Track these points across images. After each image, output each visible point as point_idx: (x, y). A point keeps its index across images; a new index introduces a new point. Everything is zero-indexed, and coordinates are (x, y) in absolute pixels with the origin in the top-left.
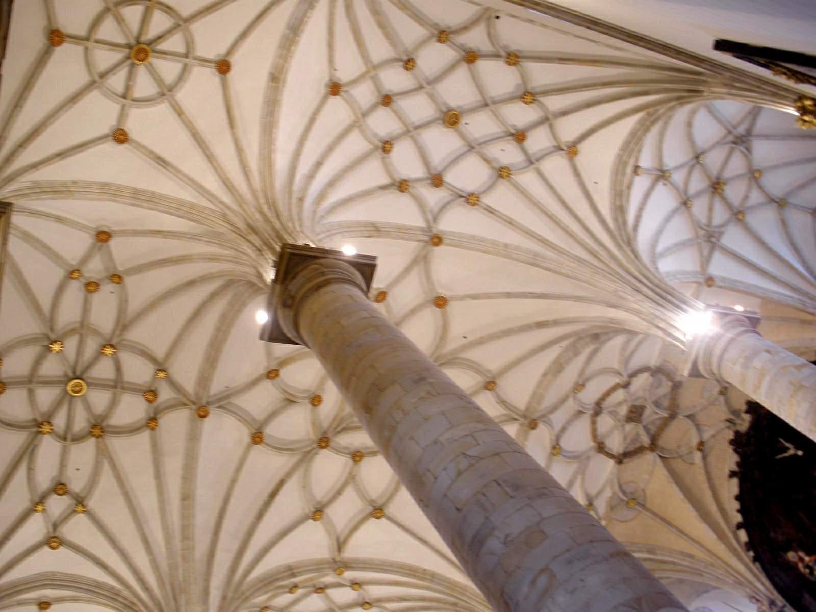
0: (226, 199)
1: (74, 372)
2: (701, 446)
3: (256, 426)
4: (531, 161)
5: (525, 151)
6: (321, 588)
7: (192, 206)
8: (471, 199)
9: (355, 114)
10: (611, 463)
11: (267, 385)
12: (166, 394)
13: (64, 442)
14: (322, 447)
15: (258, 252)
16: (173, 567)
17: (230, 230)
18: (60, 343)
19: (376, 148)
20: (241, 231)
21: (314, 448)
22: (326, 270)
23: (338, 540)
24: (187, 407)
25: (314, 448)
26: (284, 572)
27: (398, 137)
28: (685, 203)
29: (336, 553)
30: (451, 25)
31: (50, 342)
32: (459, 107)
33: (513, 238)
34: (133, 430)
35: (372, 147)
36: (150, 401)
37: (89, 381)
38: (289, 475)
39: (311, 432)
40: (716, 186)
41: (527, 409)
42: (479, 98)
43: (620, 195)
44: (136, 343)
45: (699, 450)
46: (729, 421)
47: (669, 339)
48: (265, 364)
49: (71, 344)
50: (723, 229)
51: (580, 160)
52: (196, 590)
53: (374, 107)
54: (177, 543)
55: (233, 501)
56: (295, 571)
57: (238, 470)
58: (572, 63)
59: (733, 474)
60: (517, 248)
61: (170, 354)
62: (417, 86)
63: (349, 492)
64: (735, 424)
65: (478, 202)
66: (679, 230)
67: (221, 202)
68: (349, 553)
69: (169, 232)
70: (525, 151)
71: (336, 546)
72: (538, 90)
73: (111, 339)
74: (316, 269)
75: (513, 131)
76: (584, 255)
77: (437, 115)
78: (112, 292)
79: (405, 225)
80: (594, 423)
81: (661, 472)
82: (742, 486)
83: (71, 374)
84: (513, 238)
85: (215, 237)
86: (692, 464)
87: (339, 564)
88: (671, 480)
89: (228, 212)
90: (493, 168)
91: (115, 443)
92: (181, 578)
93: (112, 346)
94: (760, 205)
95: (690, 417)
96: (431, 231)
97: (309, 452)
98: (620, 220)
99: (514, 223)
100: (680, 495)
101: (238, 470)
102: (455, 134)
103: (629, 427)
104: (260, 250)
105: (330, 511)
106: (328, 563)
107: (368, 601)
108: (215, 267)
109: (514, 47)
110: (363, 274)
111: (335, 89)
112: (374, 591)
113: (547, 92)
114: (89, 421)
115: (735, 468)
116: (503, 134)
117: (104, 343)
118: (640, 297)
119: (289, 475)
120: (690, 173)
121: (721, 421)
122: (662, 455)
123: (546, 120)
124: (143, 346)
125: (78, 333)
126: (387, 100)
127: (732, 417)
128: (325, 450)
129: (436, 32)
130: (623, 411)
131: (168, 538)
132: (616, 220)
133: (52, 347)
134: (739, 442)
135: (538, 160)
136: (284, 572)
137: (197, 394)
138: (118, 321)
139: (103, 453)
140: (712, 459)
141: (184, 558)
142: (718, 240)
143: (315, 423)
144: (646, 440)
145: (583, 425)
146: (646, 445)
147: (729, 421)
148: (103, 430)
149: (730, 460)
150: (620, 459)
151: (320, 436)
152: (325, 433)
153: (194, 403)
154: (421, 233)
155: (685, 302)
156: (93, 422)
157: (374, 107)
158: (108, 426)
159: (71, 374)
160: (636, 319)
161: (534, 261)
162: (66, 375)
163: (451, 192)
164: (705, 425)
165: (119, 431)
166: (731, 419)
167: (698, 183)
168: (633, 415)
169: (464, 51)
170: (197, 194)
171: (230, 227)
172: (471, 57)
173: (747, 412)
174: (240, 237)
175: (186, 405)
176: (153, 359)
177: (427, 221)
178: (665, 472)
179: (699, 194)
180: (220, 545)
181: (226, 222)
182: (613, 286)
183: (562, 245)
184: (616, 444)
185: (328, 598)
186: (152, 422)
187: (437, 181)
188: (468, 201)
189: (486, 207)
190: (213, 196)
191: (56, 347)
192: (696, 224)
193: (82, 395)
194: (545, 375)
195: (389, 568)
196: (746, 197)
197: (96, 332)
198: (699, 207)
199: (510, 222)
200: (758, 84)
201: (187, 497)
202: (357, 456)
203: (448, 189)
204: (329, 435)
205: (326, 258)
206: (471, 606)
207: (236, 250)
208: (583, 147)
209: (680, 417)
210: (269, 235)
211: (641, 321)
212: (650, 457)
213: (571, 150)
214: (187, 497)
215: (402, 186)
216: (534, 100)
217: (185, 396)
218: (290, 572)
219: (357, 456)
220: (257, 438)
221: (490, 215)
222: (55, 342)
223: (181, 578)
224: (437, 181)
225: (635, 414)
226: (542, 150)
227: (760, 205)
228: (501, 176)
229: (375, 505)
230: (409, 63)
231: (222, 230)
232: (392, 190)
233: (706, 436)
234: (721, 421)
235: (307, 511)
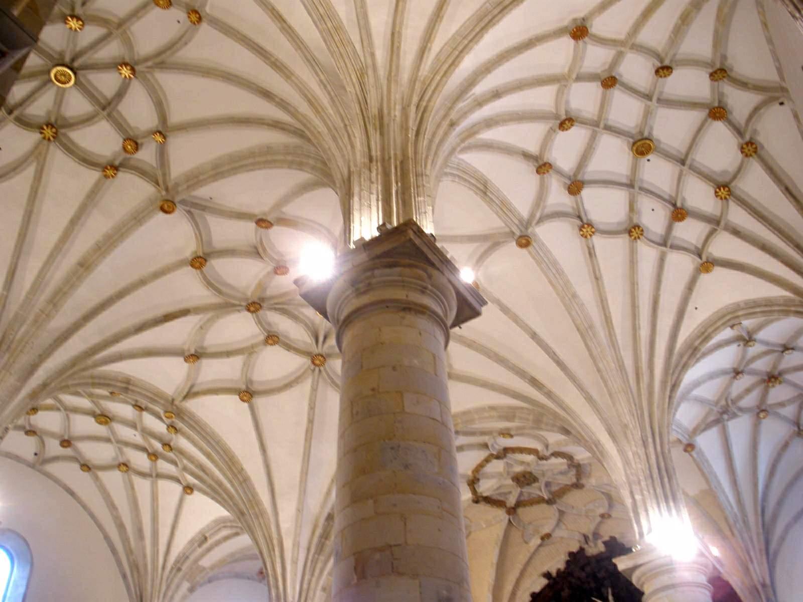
0: (381, 55)
1: (73, 60)
2: (546, 537)
3: (207, 250)
4: (665, 242)
5: (669, 228)
6: (140, 407)
7: (339, 28)
8: (586, 227)
9: (570, 70)
11: (252, 225)
12: (147, 155)
13: (6, 115)
14: (249, 310)
15: (367, 161)
16: (18, 319)
17: (356, 94)
18: (81, 23)
19: (556, 116)
20: (367, 109)
21: (240, 305)
22: (430, 287)
23: (192, 386)
24: (158, 187)
25: (240, 305)
26: (121, 382)
27: (584, 122)
28: (737, 372)
29: (180, 398)
30: (735, 69)
31: (71, 13)
32: (659, 141)
33: (585, 291)
34: (87, 161)
35: (554, 111)
36: (125, 149)
37: (82, 79)
38: (197, 310)
40: (772, 378)
42: (683, 150)
43: (704, 334)
44: (161, 87)
45: (542, 539)
46: (586, 537)
47: (632, 515)
48: (266, 209)
49: (92, 33)
50: (739, 414)
51: (705, 279)
52: (25, 359)
53: (591, 77)
55: (127, 299)
56: (131, 387)
57: (157, 275)
58: (794, 203)
59: (547, 575)
60: (582, 306)
61: (185, 127)
62: (647, 92)
64: (587, 542)
65: (589, 237)
66: (709, 391)
67: (373, 55)
68: (194, 406)
69: (290, 27)
70: (669, 228)
71: (185, 393)
72: (738, 192)
73: (137, 63)
74: (420, 278)
75: (679, 204)
76: (629, 363)
77: (634, 132)
78: (179, 22)
79: (510, 204)
80: (487, 460)
81: (498, 531)
82: (547, 587)
83: (67, 59)
84: (585, 291)
85: (334, 86)
86: (526, 543)
87: (175, 407)
88: (499, 544)
89: (370, 72)
90: (631, 219)
91: (57, 157)
92: (18, 337)
93: (133, 70)
94: (784, 418)
95: (561, 513)
96: (527, 228)
97: (234, 305)
98: (685, 359)
99: (600, 282)
101: (157, 275)
102: (631, 159)
103: (509, 482)
104: (371, 159)
105: (205, 363)
106: (166, 400)
107: (172, 444)
108: (304, 108)
109: (761, 139)
110: (457, 316)
111: (579, 31)
112: (182, 443)
113: (744, 203)
114: (49, 113)
115: (554, 573)
116: (667, 197)
117: (127, 60)
118: (641, 452)
119: (197, 310)
120: (766, 353)
121: (579, 533)
122: (511, 520)
123: (715, 223)
124: (166, 99)
125: (108, 28)
126: (609, 82)
127: (591, 537)
128: (249, 314)
129: (718, 66)
130: (518, 469)
132: (681, 356)
133: (69, 21)
134: (576, 558)
135: (672, 247)
136: (121, 382)
137: (177, 185)
138: (159, 53)
139: (37, 155)
140: (544, 551)
141: (36, 321)
142: (728, 420)
143: (262, 286)
144: (511, 501)
145: (477, 456)
147: (586, 537)
148: (56, 136)
149: (556, 563)
151: (256, 300)
152: (263, 299)
153: (167, 189)
154: (516, 222)
155: (675, 499)
156: (53, 120)
157: (591, 77)
158: (64, 135)
159: (67, 59)
160: (620, 464)
161: (585, 331)
162: (61, 54)
163: (575, 206)
164: (564, 524)
165: (71, 150)
166: (588, 537)
167: (762, 365)
168: (522, 479)
169: (720, 102)
170: (355, 19)
171: (359, 93)
172: (718, 112)
173: (605, 543)
174: (361, 117)
175: (157, 183)
176: (163, 117)
177: (532, 215)
178: (501, 533)
179: (753, 373)
180: (81, 333)
181: (360, 83)
182: (627, 419)
183: (619, 337)
184: (486, 487)
185: (141, 417)
186: (112, 168)
187: (575, 187)
188: (581, 228)
189: (591, 246)
190: (369, 36)
191: (73, 24)
192: (725, 392)
193: (63, 88)
194: (492, 408)
195: (214, 444)
196: (782, 405)
197: (128, 43)
198: (745, 381)
199: (597, 278)
201: (85, 266)
202: (272, 338)
203: (577, 202)
204: (265, 305)
205: (438, 269)
206: (253, 525)
207: (345, 126)
208: (718, 271)
209: (554, 506)
210: (395, 154)
211: (623, 473)
212: (501, 515)
213: (707, 264)
214: (85, 266)
215: (543, 167)
216: (726, 198)
217: (164, 175)
218: (124, 385)
220: (198, 262)
221: (588, 255)
222: (78, 18)
223: (18, 337)
224: (575, 187)
225: (524, 479)
226: (683, 240)
227: (784, 418)
228: (630, 232)
229: (250, 386)
230: (664, 70)
231: (349, 89)
232: (531, 164)
233: (558, 534)
234: (579, 533)
235: (186, 347)
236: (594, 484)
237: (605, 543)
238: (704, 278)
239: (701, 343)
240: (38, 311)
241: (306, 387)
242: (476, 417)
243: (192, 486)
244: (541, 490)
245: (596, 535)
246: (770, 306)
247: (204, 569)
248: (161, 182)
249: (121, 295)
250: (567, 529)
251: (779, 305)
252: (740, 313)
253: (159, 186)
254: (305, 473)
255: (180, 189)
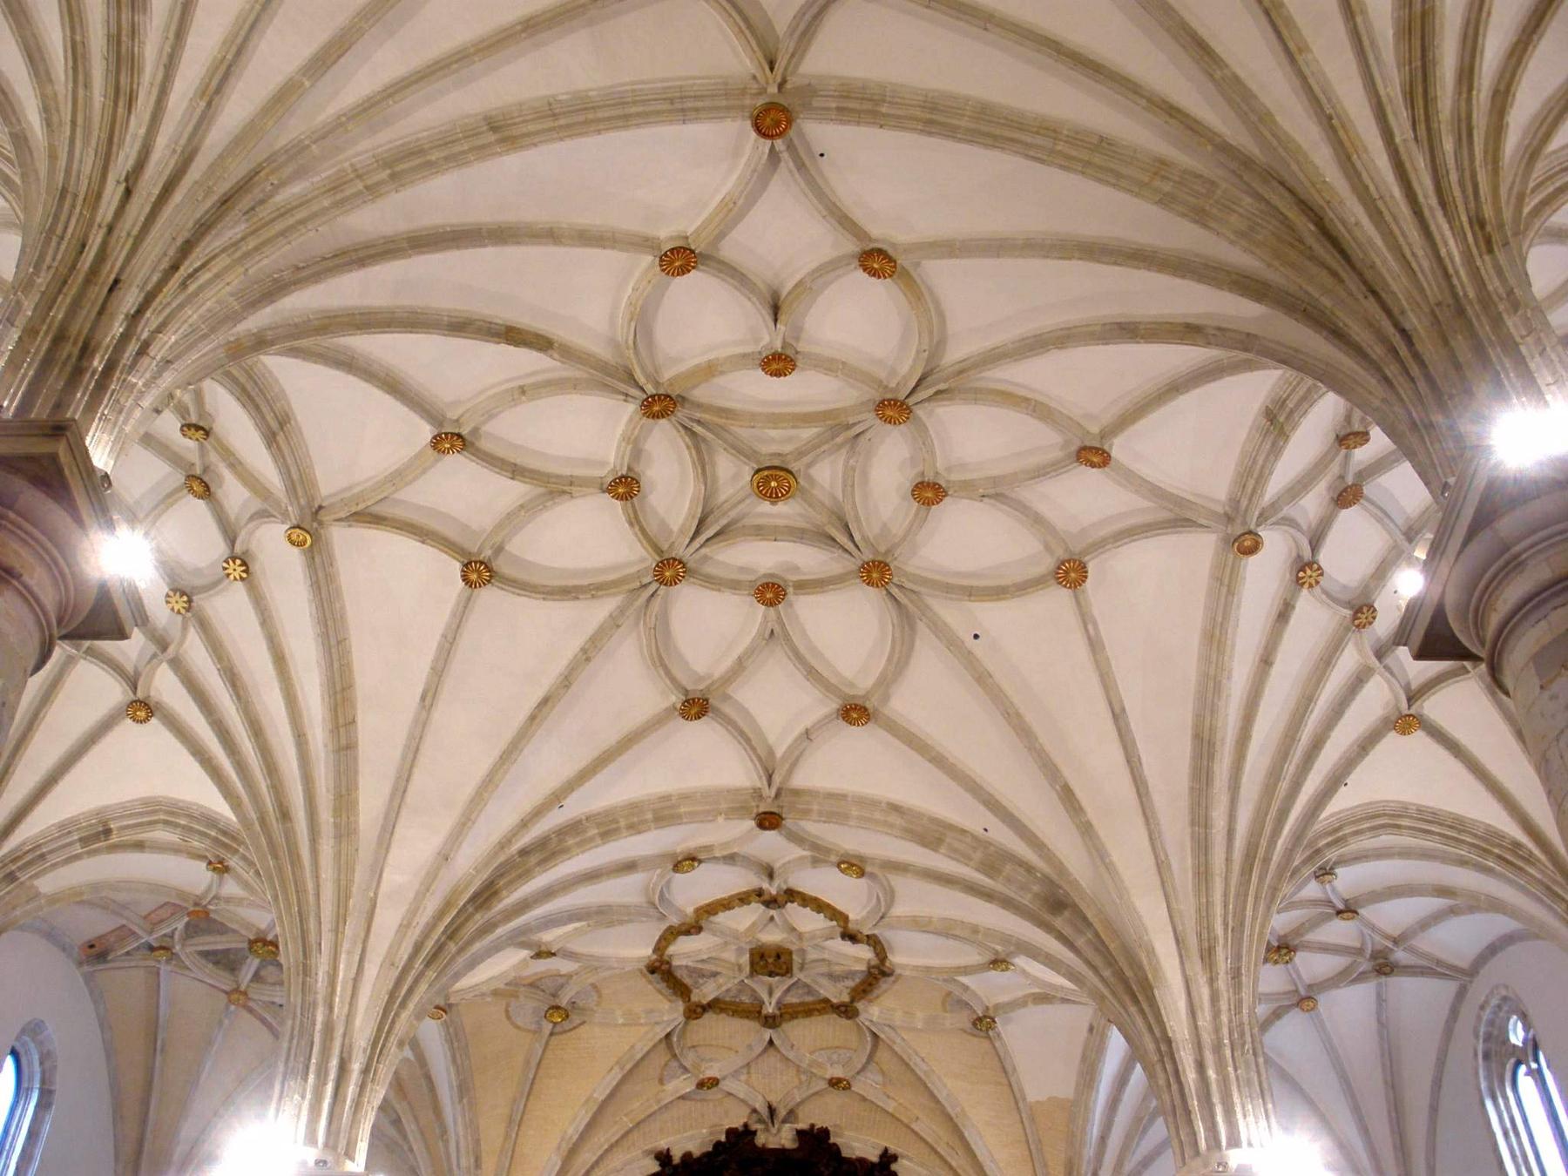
10: (645, 951)
38: (568, 353)
39: (683, 368)
41: (797, 793)
45: (701, 1085)
46: (772, 1111)
54: (365, 147)
56: (281, 438)
59: (664, 1158)
63: (514, 492)
80: (743, 899)
81: (642, 1038)
92: (282, 197)
100: (600, 1096)
115: (677, 1156)
131: (370, 109)
141: (335, 186)
144: (707, 992)
146: (694, 998)
150: (661, 970)
153: (781, 86)
184: (685, 951)
194: (895, 808)
200: (55, 239)
202: (625, 486)
204: (681, 413)
208: (1419, 738)
218: (274, 425)
219: (625, 486)
223: (282, 197)
233: (727, 1085)
236: (874, 1019)
237: (800, 1133)
238: (1392, 738)
239: (1329, 845)
240: (346, 165)
241: (599, 611)
242: (855, 812)
243: (152, 705)
244: (771, 994)
245: (791, 1115)
246: (1460, 831)
247: (37, 895)
248: (779, 67)
249: (501, 235)
250: (747, 1083)
251: (1475, 836)
252: (1405, 822)
253: (772, 69)
254: (489, 784)
255: (816, 103)
